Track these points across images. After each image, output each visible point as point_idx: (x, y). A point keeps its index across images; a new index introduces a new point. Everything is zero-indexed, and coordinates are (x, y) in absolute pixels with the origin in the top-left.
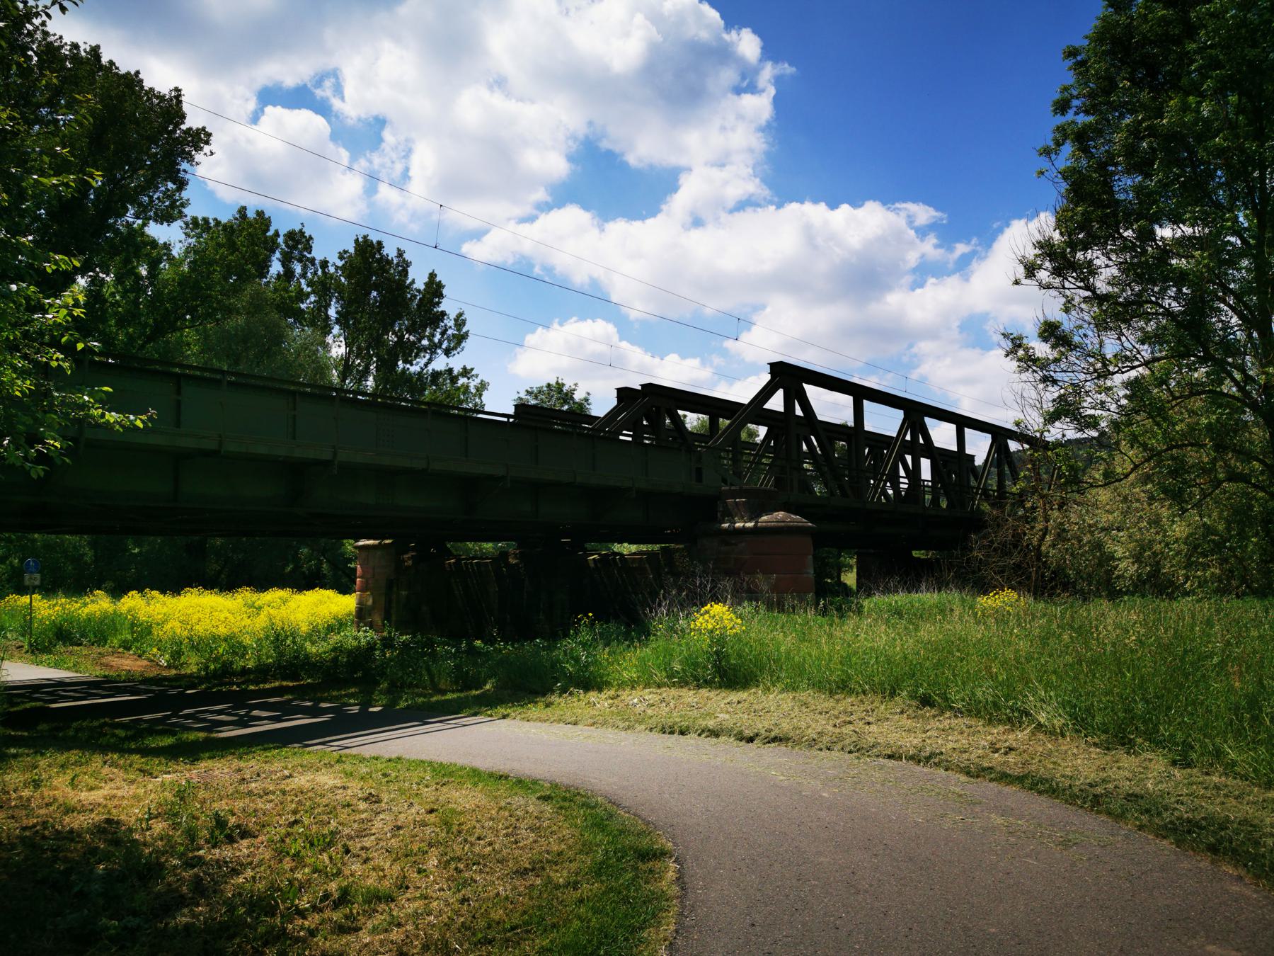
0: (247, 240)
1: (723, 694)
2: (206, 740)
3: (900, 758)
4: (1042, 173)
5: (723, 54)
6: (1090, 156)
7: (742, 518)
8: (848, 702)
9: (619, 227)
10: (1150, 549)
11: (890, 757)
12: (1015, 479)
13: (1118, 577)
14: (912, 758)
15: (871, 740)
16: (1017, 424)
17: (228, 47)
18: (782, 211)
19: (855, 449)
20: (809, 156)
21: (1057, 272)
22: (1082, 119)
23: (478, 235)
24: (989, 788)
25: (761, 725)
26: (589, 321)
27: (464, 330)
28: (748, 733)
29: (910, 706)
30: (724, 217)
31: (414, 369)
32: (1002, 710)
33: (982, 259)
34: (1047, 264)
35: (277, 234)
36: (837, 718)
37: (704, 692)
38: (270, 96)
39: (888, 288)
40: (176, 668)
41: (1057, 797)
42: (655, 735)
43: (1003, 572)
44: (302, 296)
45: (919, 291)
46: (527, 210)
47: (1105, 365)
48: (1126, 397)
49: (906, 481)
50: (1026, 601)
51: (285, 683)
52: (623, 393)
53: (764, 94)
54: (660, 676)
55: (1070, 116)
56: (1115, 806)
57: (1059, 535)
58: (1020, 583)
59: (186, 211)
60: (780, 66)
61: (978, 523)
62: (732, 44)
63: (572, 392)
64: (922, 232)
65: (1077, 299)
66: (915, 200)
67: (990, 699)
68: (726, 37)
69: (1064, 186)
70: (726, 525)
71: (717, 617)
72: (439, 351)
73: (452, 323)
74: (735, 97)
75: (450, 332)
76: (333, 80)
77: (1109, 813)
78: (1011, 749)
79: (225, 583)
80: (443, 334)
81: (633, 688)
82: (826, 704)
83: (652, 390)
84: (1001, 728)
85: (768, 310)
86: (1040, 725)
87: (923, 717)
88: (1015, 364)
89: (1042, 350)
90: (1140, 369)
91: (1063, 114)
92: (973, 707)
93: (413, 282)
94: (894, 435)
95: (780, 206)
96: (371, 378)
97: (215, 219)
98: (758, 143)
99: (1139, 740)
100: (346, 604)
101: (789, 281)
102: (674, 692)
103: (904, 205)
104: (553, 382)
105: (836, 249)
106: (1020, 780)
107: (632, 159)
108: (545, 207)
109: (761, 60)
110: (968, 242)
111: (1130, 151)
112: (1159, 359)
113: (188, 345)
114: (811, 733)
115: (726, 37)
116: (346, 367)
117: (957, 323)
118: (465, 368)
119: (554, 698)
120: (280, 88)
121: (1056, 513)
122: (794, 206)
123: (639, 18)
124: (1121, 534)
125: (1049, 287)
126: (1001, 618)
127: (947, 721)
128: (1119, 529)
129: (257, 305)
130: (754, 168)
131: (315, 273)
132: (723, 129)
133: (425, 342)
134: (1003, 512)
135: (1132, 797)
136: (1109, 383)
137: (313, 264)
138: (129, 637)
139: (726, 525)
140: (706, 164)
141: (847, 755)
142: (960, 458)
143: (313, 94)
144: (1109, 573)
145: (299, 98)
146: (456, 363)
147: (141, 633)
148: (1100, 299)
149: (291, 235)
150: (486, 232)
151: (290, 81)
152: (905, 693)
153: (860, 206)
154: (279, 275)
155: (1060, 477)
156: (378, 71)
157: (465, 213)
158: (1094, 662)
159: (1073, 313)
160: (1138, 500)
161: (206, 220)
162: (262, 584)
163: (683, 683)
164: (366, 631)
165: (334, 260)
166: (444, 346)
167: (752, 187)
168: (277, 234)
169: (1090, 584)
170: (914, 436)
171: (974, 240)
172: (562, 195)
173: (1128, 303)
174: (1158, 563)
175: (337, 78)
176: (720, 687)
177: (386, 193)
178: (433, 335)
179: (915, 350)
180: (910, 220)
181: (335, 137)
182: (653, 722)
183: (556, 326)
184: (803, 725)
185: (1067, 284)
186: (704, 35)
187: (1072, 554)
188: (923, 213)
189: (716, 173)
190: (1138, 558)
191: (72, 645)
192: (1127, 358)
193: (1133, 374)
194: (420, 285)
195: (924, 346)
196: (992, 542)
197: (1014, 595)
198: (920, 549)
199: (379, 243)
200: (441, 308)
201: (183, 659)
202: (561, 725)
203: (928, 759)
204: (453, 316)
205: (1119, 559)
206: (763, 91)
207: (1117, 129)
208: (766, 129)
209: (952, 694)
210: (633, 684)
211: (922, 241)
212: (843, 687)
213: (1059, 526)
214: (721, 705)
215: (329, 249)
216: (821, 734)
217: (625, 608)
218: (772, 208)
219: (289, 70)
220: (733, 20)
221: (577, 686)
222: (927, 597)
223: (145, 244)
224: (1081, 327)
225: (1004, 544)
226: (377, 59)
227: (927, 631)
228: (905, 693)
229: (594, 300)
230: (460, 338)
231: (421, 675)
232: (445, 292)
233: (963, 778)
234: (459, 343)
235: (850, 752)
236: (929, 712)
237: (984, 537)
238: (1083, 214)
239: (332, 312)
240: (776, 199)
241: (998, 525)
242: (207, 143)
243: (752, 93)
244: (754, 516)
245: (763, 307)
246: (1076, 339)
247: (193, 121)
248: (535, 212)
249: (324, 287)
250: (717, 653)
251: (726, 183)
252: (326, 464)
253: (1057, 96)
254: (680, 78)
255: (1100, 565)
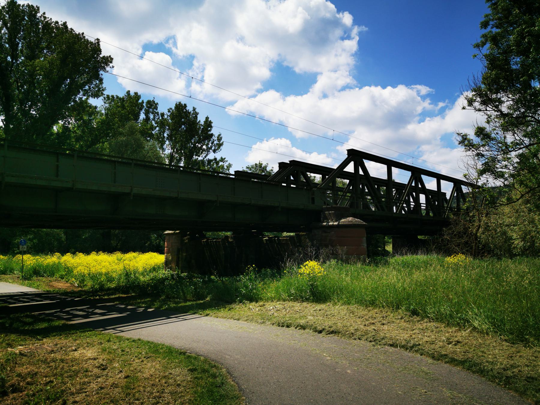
0: (130, 106)
1: (314, 305)
2: (64, 325)
3: (397, 347)
4: (476, 56)
5: (336, 23)
6: (499, 48)
7: (332, 220)
8: (374, 312)
9: (291, 99)
10: (530, 234)
11: (391, 345)
12: (465, 201)
13: (514, 248)
14: (403, 347)
15: (382, 335)
16: (465, 176)
17: (129, 27)
18: (361, 90)
19: (389, 191)
20: (373, 67)
21: (483, 103)
22: (495, 30)
23: (232, 103)
24: (444, 367)
25: (327, 323)
26: (279, 139)
27: (221, 142)
28: (319, 328)
29: (406, 315)
30: (336, 93)
31: (200, 158)
32: (454, 319)
33: (450, 109)
34: (478, 99)
35: (143, 102)
36: (367, 320)
37: (305, 304)
38: (148, 47)
39: (409, 123)
40: (81, 287)
41: (484, 376)
42: (275, 327)
43: (459, 245)
44: (152, 128)
45: (422, 123)
46: (253, 92)
47: (506, 147)
48: (517, 163)
49: (413, 204)
50: (470, 259)
51: (121, 295)
52: (281, 165)
53: (354, 40)
54: (285, 296)
55: (489, 29)
56: (520, 385)
57: (486, 228)
58: (467, 251)
59: (104, 92)
60: (361, 27)
61: (447, 223)
62: (340, 19)
63: (266, 167)
64: (424, 98)
65: (493, 117)
66: (420, 84)
67: (448, 312)
68: (338, 16)
69: (486, 63)
70: (325, 224)
71: (312, 267)
72: (211, 151)
73: (216, 138)
74: (341, 41)
75: (215, 142)
76: (173, 40)
77: (516, 391)
78: (458, 342)
79: (110, 250)
80: (212, 143)
81: (272, 301)
82: (363, 313)
83: (294, 163)
84: (454, 329)
85: (356, 133)
86: (475, 328)
87: (412, 321)
88: (464, 147)
89: (476, 140)
90: (524, 149)
91: (485, 28)
92: (439, 317)
93: (200, 121)
94: (407, 183)
95: (360, 88)
96: (182, 163)
97: (117, 96)
98: (351, 61)
99: (532, 339)
100: (158, 259)
101: (365, 120)
102: (291, 304)
103: (415, 86)
104: (258, 163)
105: (386, 106)
106: (462, 363)
107: (297, 70)
108: (260, 91)
109: (353, 25)
110: (444, 102)
111: (518, 44)
112: (533, 144)
113: (105, 149)
114: (352, 330)
115: (338, 16)
116: (171, 157)
117: (440, 137)
118: (222, 158)
119: (233, 306)
120: (152, 44)
121: (484, 218)
122: (367, 88)
123: (300, 9)
124: (515, 228)
125: (480, 110)
126: (456, 268)
127: (425, 324)
128: (514, 226)
129: (132, 131)
130: (349, 72)
131: (159, 118)
132: (336, 55)
133: (204, 147)
134: (459, 218)
135: (530, 379)
136: (509, 156)
137: (158, 115)
138: (64, 273)
139: (325, 224)
140: (329, 71)
141: (368, 343)
142: (438, 194)
143: (164, 46)
144: (510, 246)
145: (159, 48)
146: (218, 156)
147: (69, 271)
148: (503, 115)
149: (149, 102)
150: (236, 102)
151: (156, 41)
152: (403, 308)
153: (396, 87)
154: (144, 119)
155: (486, 201)
156: (192, 35)
157: (226, 95)
158: (505, 293)
159: (491, 123)
160: (523, 212)
161: (113, 96)
162: (125, 251)
163: (295, 299)
164: (168, 271)
165: (166, 112)
166: (213, 149)
167: (349, 80)
168: (143, 102)
169: (501, 251)
170: (416, 184)
171: (447, 101)
172: (268, 86)
173: (517, 118)
174: (534, 241)
175: (175, 39)
176: (313, 302)
177: (195, 87)
178: (208, 144)
179: (420, 149)
180: (418, 92)
181: (174, 64)
182: (275, 320)
183: (265, 141)
184: (348, 324)
185: (488, 109)
186: (328, 15)
187: (492, 237)
188: (424, 90)
189: (333, 75)
190: (523, 239)
191: (40, 276)
192: (517, 144)
193: (521, 151)
194: (202, 123)
195: (425, 147)
196: (454, 231)
197: (463, 257)
198: (421, 235)
199: (185, 105)
200: (212, 132)
201: (85, 283)
202: (232, 320)
203: (412, 347)
204: (216, 136)
205: (514, 239)
206: (353, 38)
207: (512, 33)
208: (355, 55)
209: (429, 309)
210: (272, 299)
211: (424, 101)
212: (373, 303)
213: (483, 225)
214: (311, 312)
215: (163, 109)
216: (356, 330)
217: (272, 261)
218: (357, 89)
219: (155, 36)
220: (340, 9)
221: (247, 300)
222: (421, 257)
223: (87, 106)
224: (495, 130)
225: (459, 233)
226: (191, 30)
227: (417, 276)
228: (403, 308)
229: (280, 130)
230: (220, 145)
231: (179, 293)
232: (213, 125)
233: (430, 361)
234: (219, 147)
235: (370, 341)
236: (416, 318)
237: (451, 229)
238: (495, 75)
239: (165, 135)
240: (359, 85)
241: (457, 224)
242: (111, 62)
243: (349, 40)
244: (338, 219)
245: (354, 132)
246: (493, 135)
247: (105, 53)
248: (256, 93)
249: (162, 124)
250: (312, 285)
251: (337, 79)
252: (128, 194)
253: (483, 19)
254: (318, 34)
255: (505, 242)
